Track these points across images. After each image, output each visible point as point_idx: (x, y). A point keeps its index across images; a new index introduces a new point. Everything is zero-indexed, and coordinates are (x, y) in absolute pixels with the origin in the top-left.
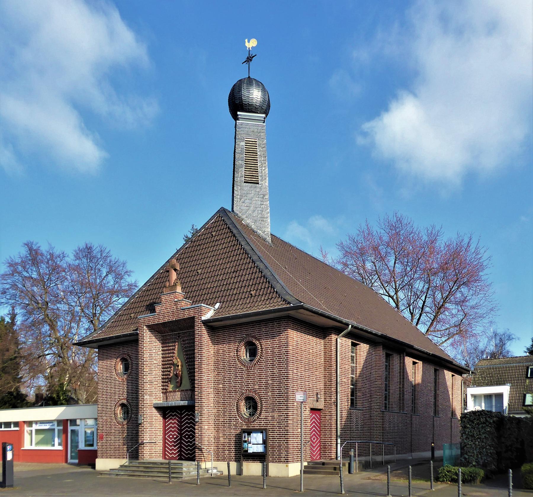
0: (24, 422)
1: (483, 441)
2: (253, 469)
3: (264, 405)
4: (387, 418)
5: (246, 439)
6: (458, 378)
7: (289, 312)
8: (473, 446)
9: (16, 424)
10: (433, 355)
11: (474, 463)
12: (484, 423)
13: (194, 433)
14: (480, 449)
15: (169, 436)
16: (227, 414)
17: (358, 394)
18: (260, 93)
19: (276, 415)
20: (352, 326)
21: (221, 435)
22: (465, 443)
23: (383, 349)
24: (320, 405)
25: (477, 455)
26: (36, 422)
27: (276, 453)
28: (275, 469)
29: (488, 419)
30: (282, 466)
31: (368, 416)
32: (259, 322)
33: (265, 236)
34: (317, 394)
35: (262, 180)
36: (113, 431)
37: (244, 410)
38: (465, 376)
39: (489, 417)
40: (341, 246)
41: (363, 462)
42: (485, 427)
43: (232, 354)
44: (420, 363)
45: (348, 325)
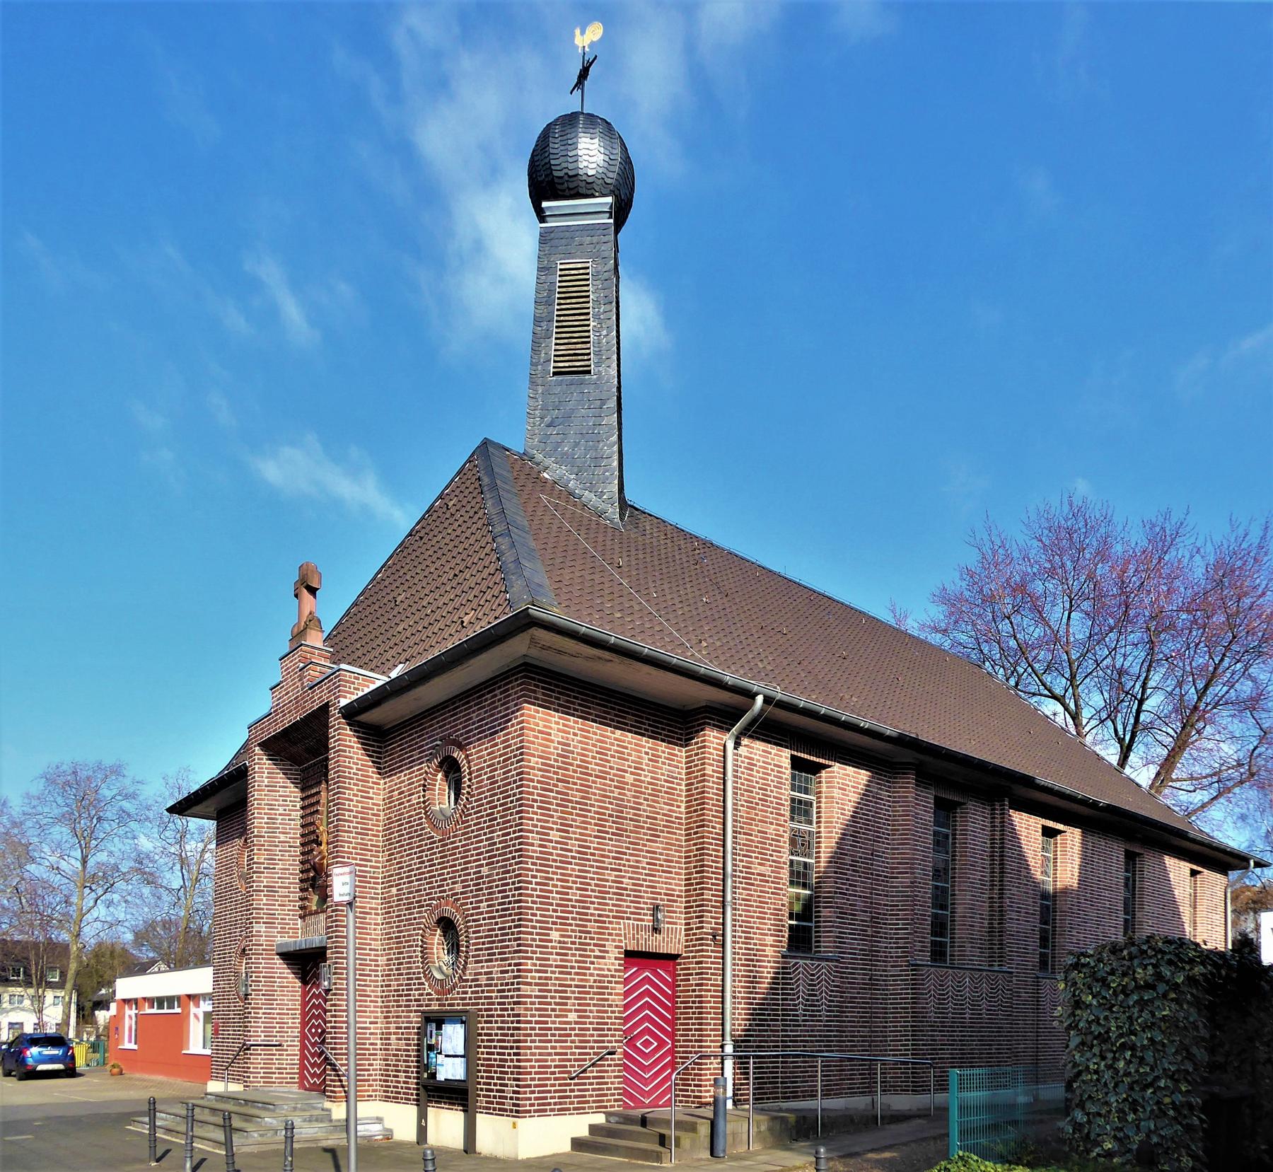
0: (144, 999)
1: (1142, 1059)
2: (446, 1126)
3: (471, 939)
4: (930, 984)
5: (433, 1041)
6: (1213, 881)
8: (1107, 1075)
9: (170, 1001)
10: (1110, 809)
11: (1108, 1146)
12: (1149, 986)
14: (1131, 1089)
17: (825, 912)
18: (596, 141)
20: (768, 700)
22: (1075, 1065)
23: (918, 784)
24: (672, 940)
25: (1120, 1111)
28: (494, 1134)
29: (1166, 971)
30: (504, 1122)
33: (602, 506)
34: (656, 908)
35: (598, 364)
37: (441, 956)
38: (1234, 875)
39: (1170, 962)
40: (944, 597)
41: (792, 1117)
42: (1151, 1001)
44: (1072, 837)
45: (753, 696)
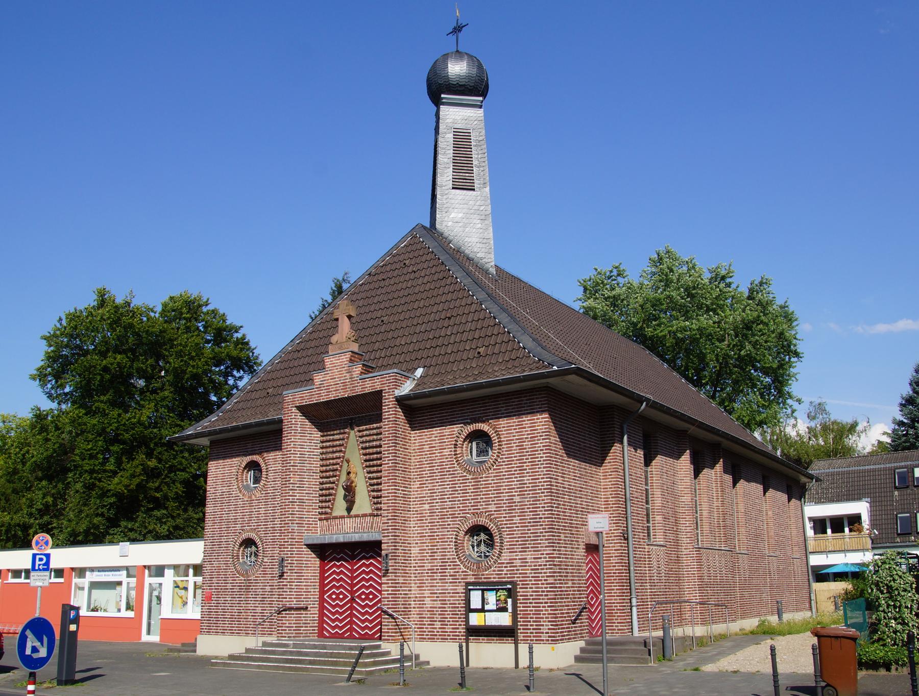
0: (72, 569)
7: (550, 380)
13: (380, 592)
15: (330, 597)
16: (438, 556)
19: (529, 556)
21: (427, 593)
26: (92, 570)
27: (532, 625)
31: (674, 557)
32: (495, 397)
36: (229, 586)
43: (446, 452)
